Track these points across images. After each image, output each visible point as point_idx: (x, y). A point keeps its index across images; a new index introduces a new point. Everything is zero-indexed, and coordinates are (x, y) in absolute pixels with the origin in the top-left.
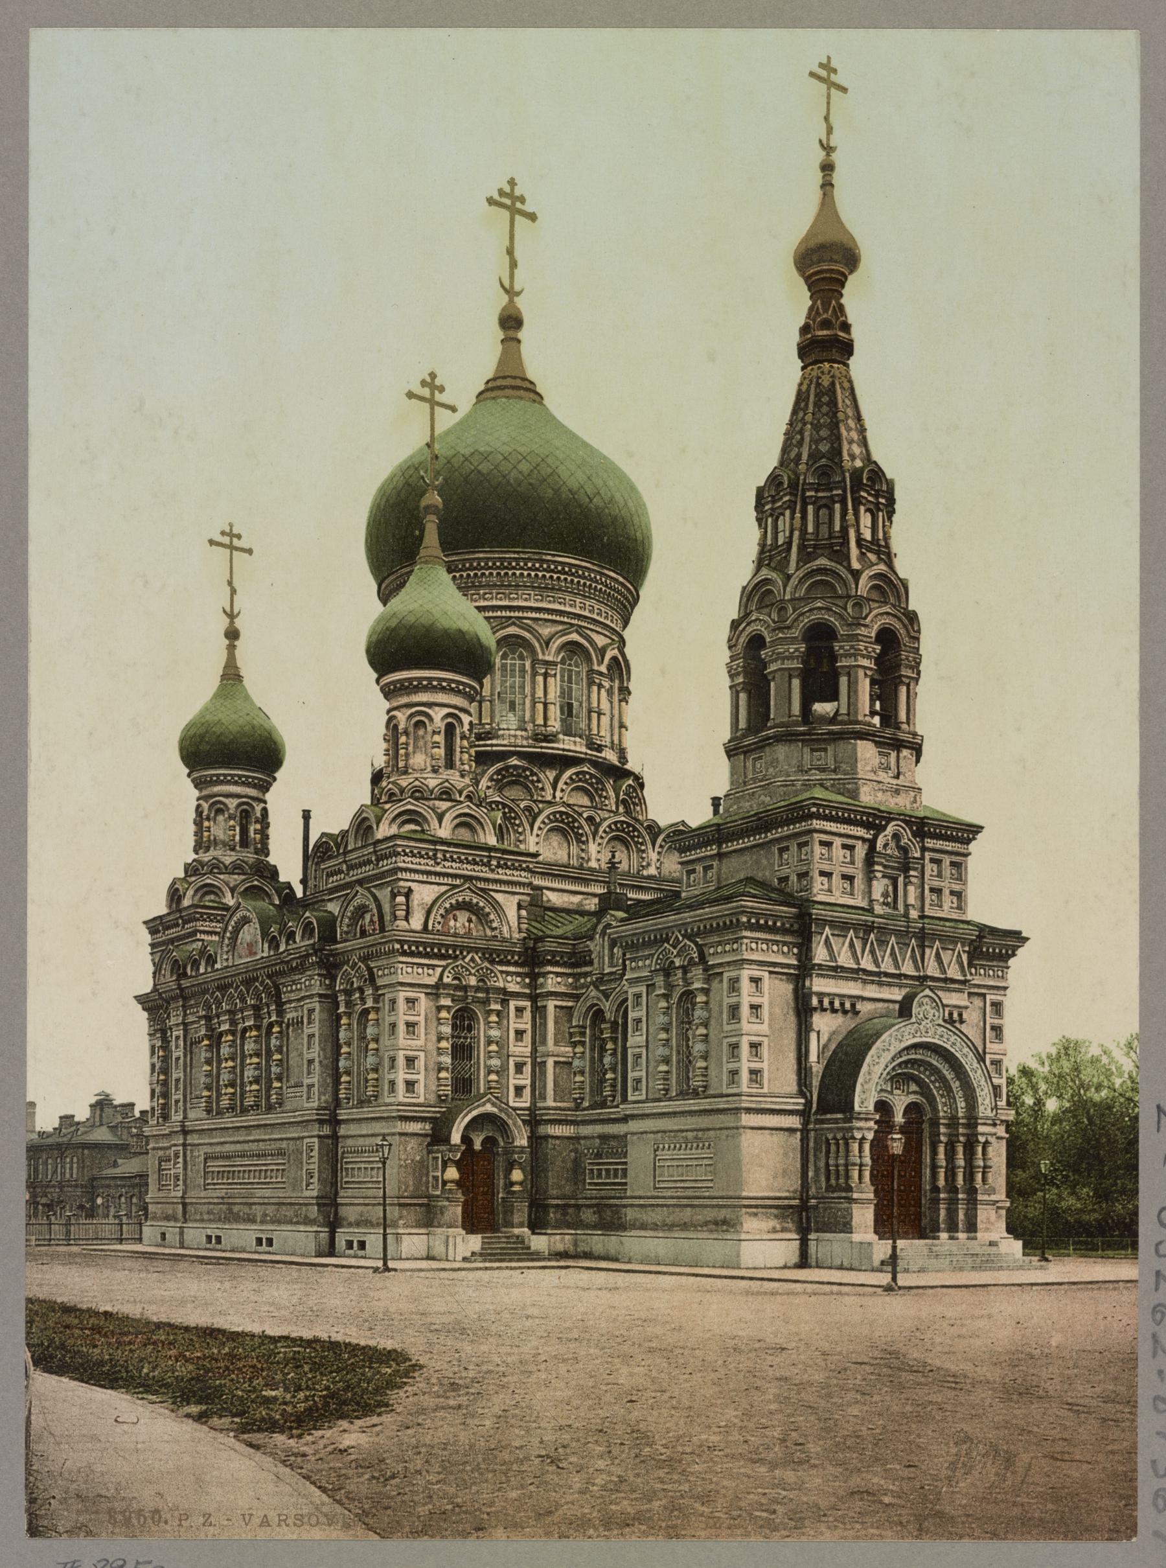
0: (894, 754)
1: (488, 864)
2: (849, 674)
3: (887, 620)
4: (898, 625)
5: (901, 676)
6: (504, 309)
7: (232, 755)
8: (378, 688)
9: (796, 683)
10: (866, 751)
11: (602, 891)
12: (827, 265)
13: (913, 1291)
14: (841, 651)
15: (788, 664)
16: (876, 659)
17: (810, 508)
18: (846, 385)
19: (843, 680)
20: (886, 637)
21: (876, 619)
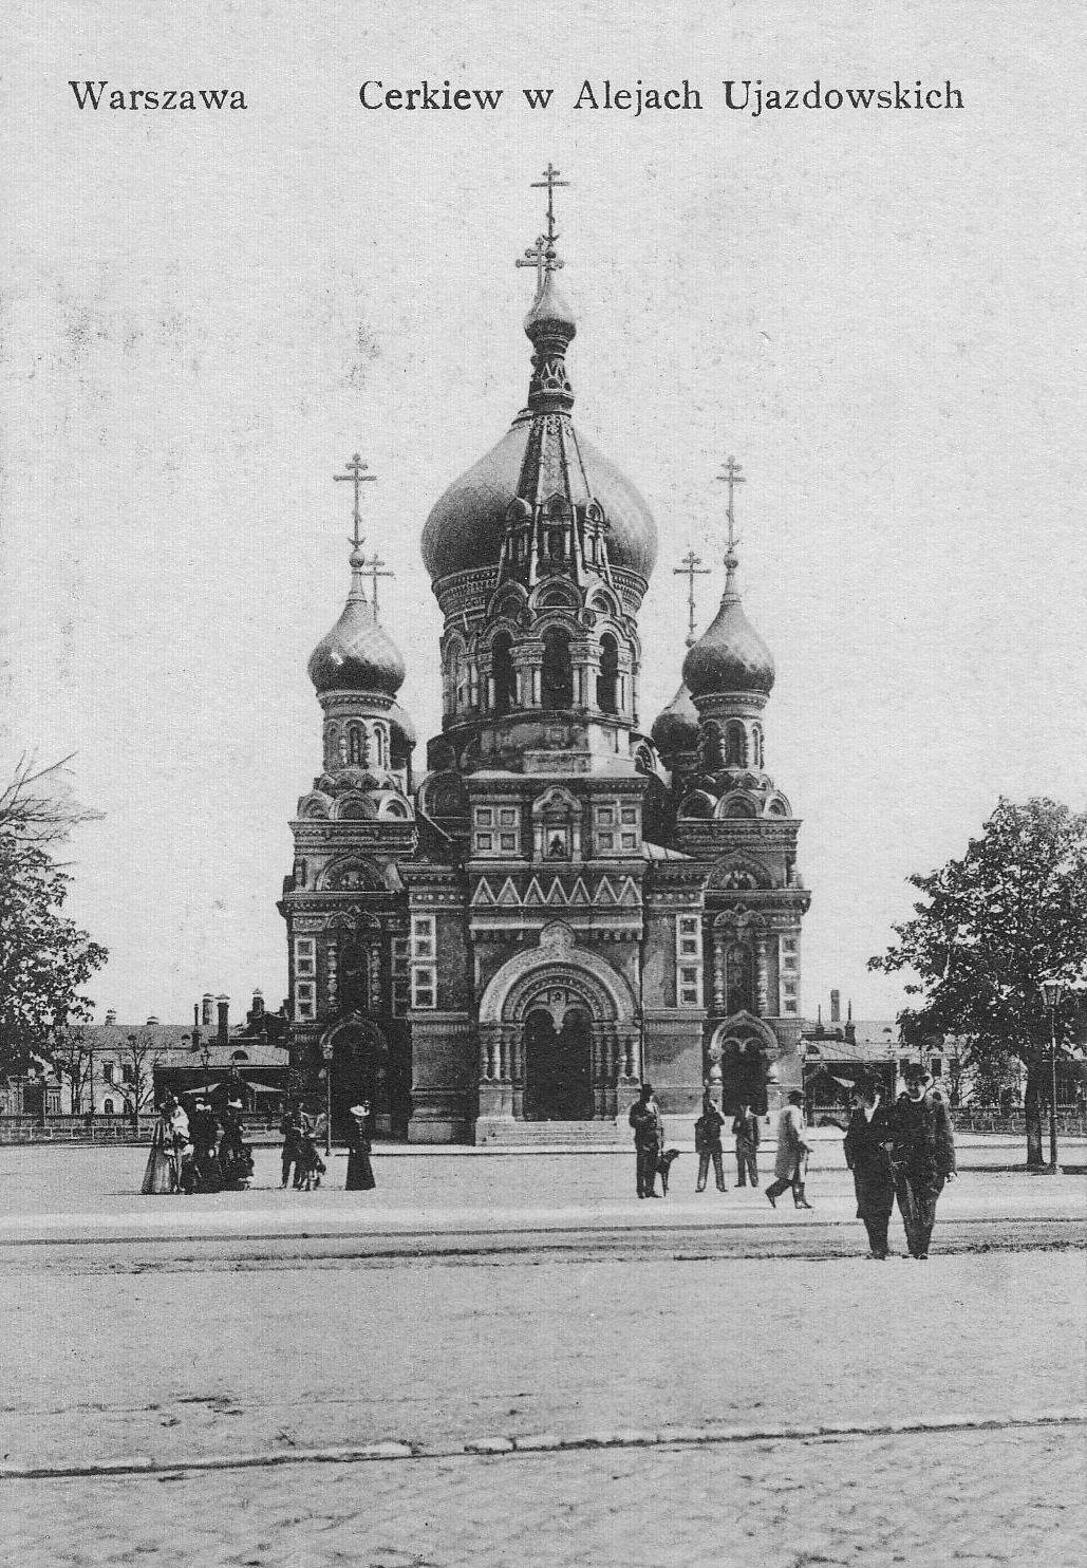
0: (613, 735)
1: (372, 835)
2: (580, 670)
3: (607, 626)
4: (615, 630)
5: (617, 671)
6: (532, 313)
7: (352, 681)
8: (721, 599)
9: (538, 675)
10: (594, 732)
11: (752, 791)
12: (549, 336)
13: (191, 1397)
14: (574, 652)
15: (532, 660)
16: (601, 658)
17: (546, 534)
18: (570, 433)
19: (576, 674)
20: (608, 641)
21: (601, 628)
